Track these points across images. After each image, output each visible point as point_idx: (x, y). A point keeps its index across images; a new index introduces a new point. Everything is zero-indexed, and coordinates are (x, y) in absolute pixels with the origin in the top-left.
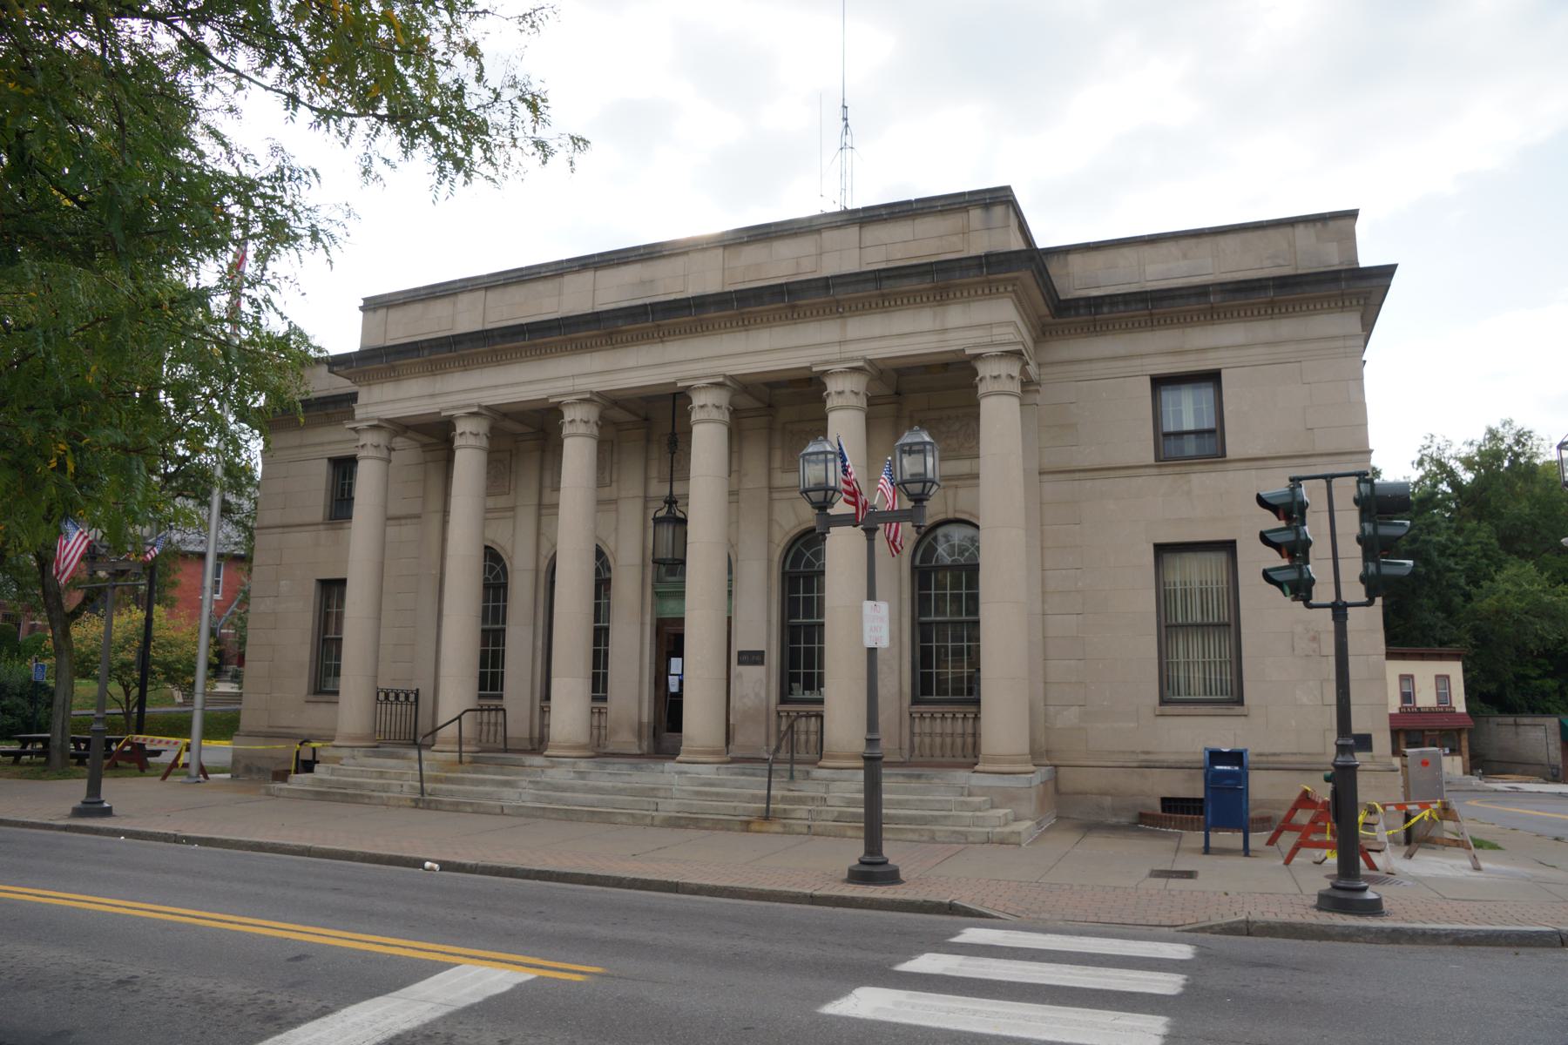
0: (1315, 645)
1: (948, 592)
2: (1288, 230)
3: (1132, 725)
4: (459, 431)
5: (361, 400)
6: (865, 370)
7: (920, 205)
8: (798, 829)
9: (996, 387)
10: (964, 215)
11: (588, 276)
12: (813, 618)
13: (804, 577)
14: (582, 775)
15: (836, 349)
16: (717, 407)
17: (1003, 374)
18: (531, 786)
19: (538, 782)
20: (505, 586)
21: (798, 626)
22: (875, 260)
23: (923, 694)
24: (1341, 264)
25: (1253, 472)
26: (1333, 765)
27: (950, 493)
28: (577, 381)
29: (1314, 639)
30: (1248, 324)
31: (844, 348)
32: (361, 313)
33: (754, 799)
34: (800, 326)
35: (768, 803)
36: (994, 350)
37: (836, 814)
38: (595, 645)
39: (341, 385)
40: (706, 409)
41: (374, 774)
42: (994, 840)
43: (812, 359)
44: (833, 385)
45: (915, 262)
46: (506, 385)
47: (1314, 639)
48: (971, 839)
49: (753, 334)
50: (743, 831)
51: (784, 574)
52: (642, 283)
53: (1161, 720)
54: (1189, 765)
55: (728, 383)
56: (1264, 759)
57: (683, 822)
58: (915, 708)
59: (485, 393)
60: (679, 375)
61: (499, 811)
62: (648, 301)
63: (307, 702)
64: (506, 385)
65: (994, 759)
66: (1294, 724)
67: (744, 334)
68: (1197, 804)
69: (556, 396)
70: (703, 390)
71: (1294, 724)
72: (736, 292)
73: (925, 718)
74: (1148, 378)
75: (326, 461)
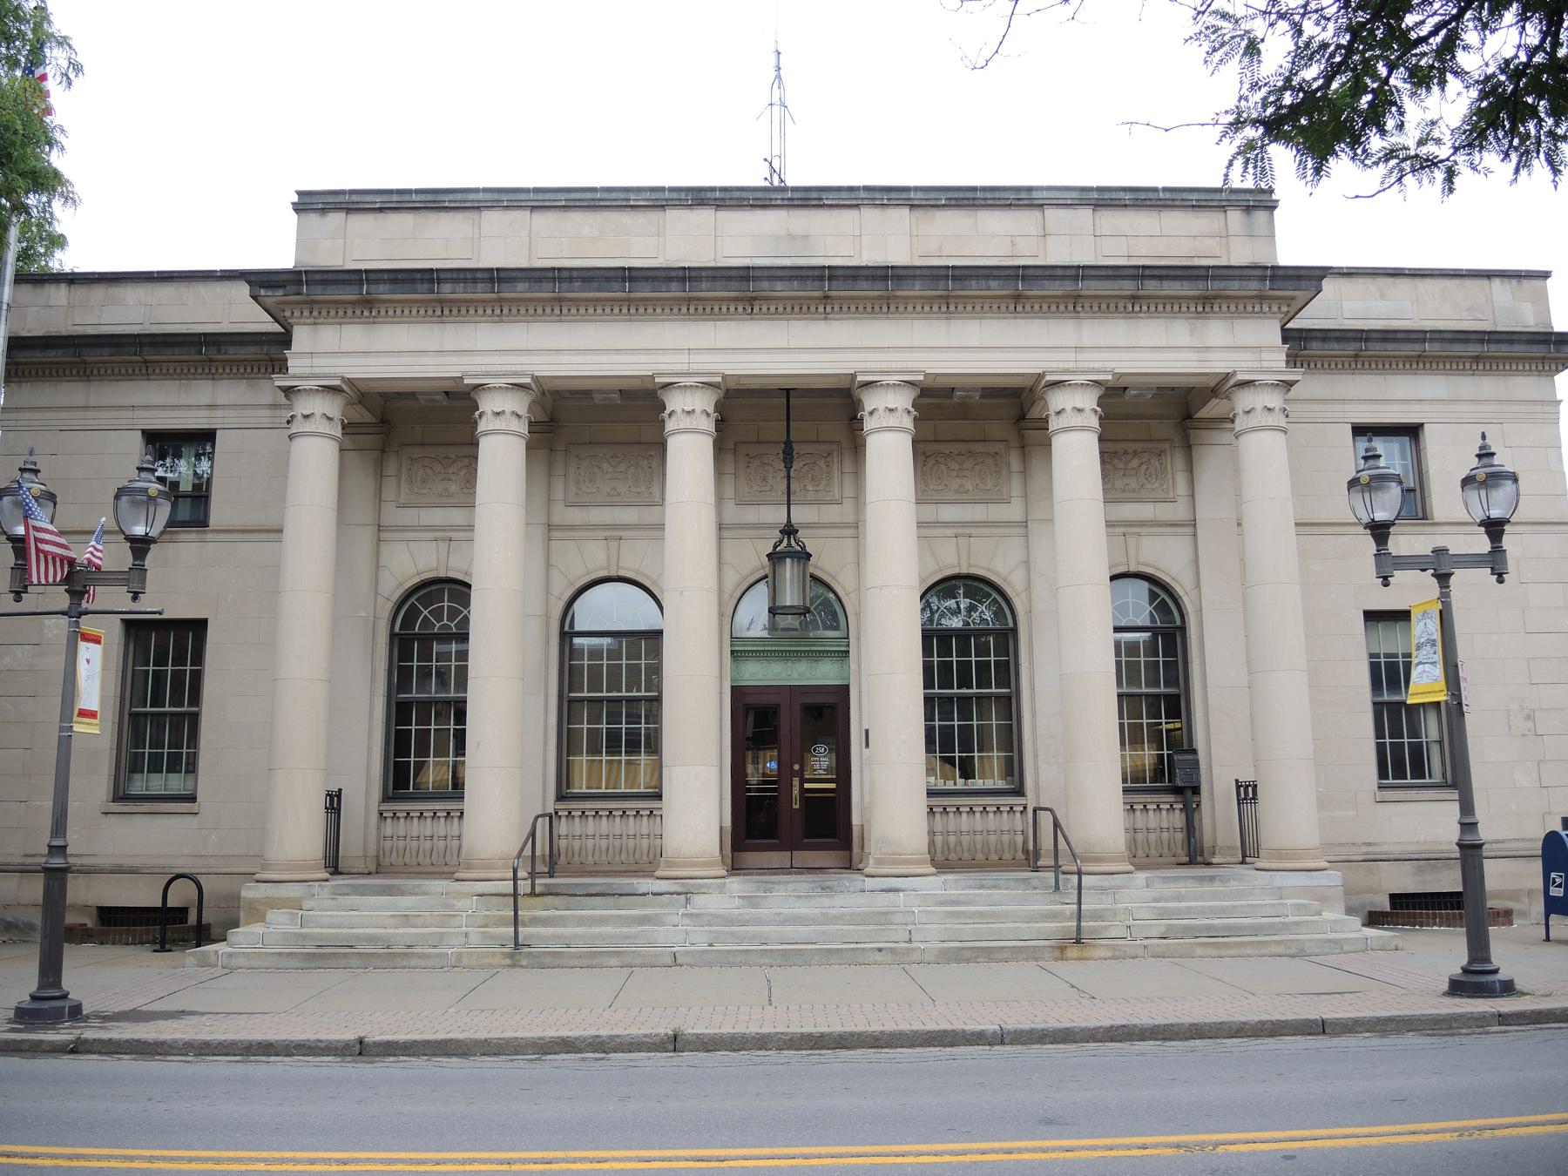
0: (1531, 724)
2: (1485, 282)
3: (1351, 813)
4: (868, 408)
6: (343, 391)
7: (1168, 195)
8: (1133, 952)
9: (498, 424)
10: (1220, 215)
11: (705, 216)
13: (1162, 634)
14: (750, 901)
15: (1072, 356)
16: (330, 419)
18: (687, 921)
19: (698, 915)
20: (1014, 631)
22: (1114, 253)
24: (1537, 325)
25: (1461, 537)
27: (1131, 540)
28: (695, 358)
29: (1528, 717)
30: (1450, 377)
31: (1080, 356)
32: (295, 216)
33: (535, 921)
35: (1079, 919)
37: (1163, 929)
39: (255, 319)
40: (502, 418)
41: (392, 921)
42: (1374, 947)
43: (1234, 365)
44: (488, 404)
47: (1528, 717)
48: (1346, 948)
50: (1056, 959)
51: (393, 635)
52: (792, 237)
54: (1416, 856)
55: (345, 387)
57: (967, 954)
58: (385, 807)
59: (535, 359)
60: (1054, 366)
61: (669, 960)
62: (827, 262)
65: (1281, 854)
66: (1514, 808)
67: (943, 323)
68: (1455, 899)
69: (477, 376)
70: (689, 391)
71: (1514, 808)
74: (1350, 425)
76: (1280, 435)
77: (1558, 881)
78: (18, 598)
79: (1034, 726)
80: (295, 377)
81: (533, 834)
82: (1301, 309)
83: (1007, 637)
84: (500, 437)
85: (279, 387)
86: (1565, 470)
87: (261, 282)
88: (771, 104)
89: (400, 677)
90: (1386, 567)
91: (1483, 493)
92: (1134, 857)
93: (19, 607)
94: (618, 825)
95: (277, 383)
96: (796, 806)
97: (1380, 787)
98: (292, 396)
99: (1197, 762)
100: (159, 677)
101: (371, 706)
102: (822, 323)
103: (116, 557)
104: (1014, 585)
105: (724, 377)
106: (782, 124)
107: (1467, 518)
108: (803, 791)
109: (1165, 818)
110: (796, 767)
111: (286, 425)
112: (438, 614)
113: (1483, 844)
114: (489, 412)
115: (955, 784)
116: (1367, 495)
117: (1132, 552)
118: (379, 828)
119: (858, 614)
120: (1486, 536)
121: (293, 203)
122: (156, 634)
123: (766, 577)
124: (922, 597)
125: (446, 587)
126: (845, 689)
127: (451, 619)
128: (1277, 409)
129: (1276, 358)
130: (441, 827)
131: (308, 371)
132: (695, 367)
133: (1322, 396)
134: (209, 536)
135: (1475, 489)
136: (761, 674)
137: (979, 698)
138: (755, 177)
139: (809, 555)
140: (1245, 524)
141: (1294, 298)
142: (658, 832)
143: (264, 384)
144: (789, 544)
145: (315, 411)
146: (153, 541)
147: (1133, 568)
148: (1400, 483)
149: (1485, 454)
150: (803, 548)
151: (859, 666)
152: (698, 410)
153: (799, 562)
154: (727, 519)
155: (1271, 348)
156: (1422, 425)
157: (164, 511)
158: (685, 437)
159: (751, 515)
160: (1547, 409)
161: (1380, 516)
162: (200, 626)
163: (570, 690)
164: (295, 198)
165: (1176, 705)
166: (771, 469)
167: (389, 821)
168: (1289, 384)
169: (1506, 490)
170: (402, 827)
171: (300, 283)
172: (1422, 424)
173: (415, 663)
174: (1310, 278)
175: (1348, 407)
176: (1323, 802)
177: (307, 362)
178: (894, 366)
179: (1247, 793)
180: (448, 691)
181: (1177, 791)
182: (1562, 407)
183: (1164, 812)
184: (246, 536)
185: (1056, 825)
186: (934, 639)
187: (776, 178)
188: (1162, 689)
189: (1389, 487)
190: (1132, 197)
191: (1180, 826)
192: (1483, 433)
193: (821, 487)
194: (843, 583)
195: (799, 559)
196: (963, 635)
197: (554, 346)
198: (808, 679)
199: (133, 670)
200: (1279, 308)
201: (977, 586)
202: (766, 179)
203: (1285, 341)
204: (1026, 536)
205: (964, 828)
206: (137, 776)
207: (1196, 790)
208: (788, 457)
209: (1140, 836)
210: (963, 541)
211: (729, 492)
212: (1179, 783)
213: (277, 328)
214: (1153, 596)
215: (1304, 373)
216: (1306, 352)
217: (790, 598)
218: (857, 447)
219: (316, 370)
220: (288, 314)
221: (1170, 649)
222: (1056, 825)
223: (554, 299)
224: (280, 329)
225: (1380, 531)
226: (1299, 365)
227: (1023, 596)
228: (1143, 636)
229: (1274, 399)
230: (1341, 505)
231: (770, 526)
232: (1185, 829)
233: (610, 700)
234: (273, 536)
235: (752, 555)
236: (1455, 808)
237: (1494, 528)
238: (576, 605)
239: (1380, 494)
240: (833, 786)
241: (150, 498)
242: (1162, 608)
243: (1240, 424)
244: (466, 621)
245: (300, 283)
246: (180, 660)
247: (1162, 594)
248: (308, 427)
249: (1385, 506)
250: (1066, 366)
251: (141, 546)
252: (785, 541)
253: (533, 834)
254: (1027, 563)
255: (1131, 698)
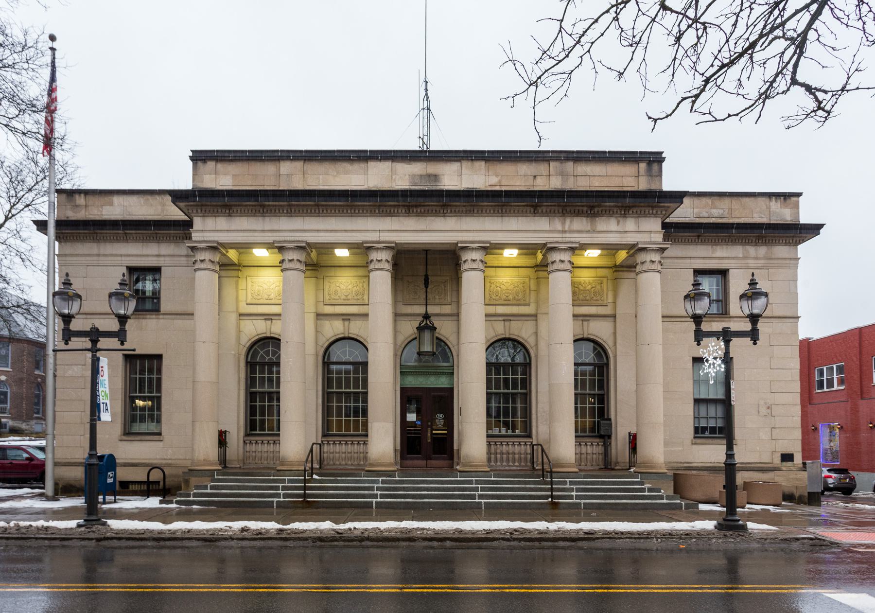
0: (769, 411)
1: (588, 378)
3: (680, 449)
4: (463, 259)
5: (195, 227)
12: (500, 389)
15: (560, 235)
17: (295, 259)
21: (255, 393)
23: (251, 430)
26: (724, 463)
27: (585, 323)
29: (768, 408)
34: (354, 219)
36: (203, 245)
38: (279, 405)
39: (175, 213)
43: (637, 240)
45: (606, 189)
46: (327, 231)
47: (768, 408)
49: (506, 219)
51: (247, 362)
53: (695, 446)
56: (744, 465)
59: (307, 234)
63: (121, 440)
64: (327, 231)
67: (500, 219)
70: (379, 251)
71: (758, 449)
72: (596, 191)
73: (246, 443)
75: (125, 268)
76: (659, 274)
77: (111, 475)
78: (67, 343)
79: (537, 407)
80: (196, 242)
81: (311, 450)
82: (672, 213)
83: (527, 366)
84: (292, 271)
85: (188, 246)
86: (798, 291)
87: (178, 196)
88: (423, 109)
89: (251, 381)
90: (699, 335)
91: (750, 302)
92: (580, 465)
93: (67, 347)
94: (350, 448)
95: (187, 245)
96: (429, 441)
97: (695, 438)
98: (194, 251)
99: (611, 424)
100: (142, 381)
101: (239, 393)
102: (442, 218)
103: (113, 325)
104: (530, 342)
105: (396, 244)
106: (428, 119)
107: (742, 315)
108: (432, 434)
109: (594, 449)
110: (429, 424)
111: (193, 265)
112: (267, 353)
113: (736, 464)
114: (287, 260)
115: (500, 432)
116: (693, 303)
117: (585, 329)
118: (244, 448)
119: (458, 356)
120: (693, 323)
121: (190, 157)
122: (157, 362)
123: (415, 338)
124: (486, 350)
125: (271, 341)
126: (451, 390)
127: (273, 355)
128: (657, 262)
129: (658, 237)
130: (271, 448)
131: (201, 239)
132: (382, 239)
133: (680, 255)
134: (161, 317)
135: (745, 300)
136: (413, 382)
137: (513, 394)
138: (413, 144)
139: (435, 328)
140: (638, 316)
141: (668, 207)
142: (278, 450)
143: (181, 245)
144: (426, 323)
145: (206, 258)
146: (73, 317)
147: (585, 336)
148: (709, 297)
149: (753, 283)
150: (433, 325)
151: (458, 379)
152: (384, 259)
153: (431, 331)
154: (399, 311)
155: (656, 232)
156: (728, 270)
157: (133, 304)
158: (469, 273)
159: (409, 310)
160: (792, 262)
161: (699, 312)
162: (159, 357)
163: (328, 388)
164: (191, 154)
165: (602, 399)
166: (419, 288)
167: (248, 445)
168: (662, 250)
169: (762, 301)
170: (253, 447)
171: (195, 196)
172: (728, 270)
173: (258, 375)
174: (678, 197)
175: (692, 261)
176: (666, 444)
177: (201, 234)
178: (476, 239)
179: (633, 440)
180: (273, 388)
181: (601, 437)
182: (800, 261)
183: (594, 446)
184: (178, 317)
185: (543, 450)
186: (492, 368)
187: (425, 146)
188: (597, 392)
189: (704, 299)
190: (565, 156)
191: (601, 452)
192: (753, 273)
193: (442, 296)
194: (451, 341)
195: (431, 330)
196: (505, 365)
197: (316, 228)
198: (439, 384)
199: (130, 377)
200: (661, 212)
201: (517, 343)
202: (420, 147)
203: (663, 228)
204: (536, 321)
205: (516, 451)
206: (134, 424)
207: (610, 437)
208: (426, 283)
209: (589, 457)
210: (507, 323)
211: (400, 298)
212: (602, 433)
213: (186, 218)
214: (595, 349)
215: (671, 244)
216: (800, 235)
217: (427, 347)
218: (457, 279)
219: (205, 239)
220: (190, 211)
221: (601, 374)
222: (543, 450)
223: (315, 205)
224: (189, 219)
225: (697, 319)
226: (670, 240)
227: (534, 348)
228: (588, 368)
229: (656, 257)
230: (681, 308)
231: (418, 315)
232: (603, 455)
233: (355, 393)
234: (190, 317)
235: (409, 328)
236: (724, 447)
237: (754, 318)
238: (331, 349)
239: (699, 302)
240: (446, 432)
241: (125, 297)
242: (598, 355)
243: (638, 269)
244: (279, 357)
245: (195, 196)
246: (151, 371)
247: (599, 348)
248: (202, 266)
249: (702, 306)
250: (346, 234)
251: (123, 319)
252: (425, 322)
253: (311, 450)
254: (536, 333)
255: (582, 396)
